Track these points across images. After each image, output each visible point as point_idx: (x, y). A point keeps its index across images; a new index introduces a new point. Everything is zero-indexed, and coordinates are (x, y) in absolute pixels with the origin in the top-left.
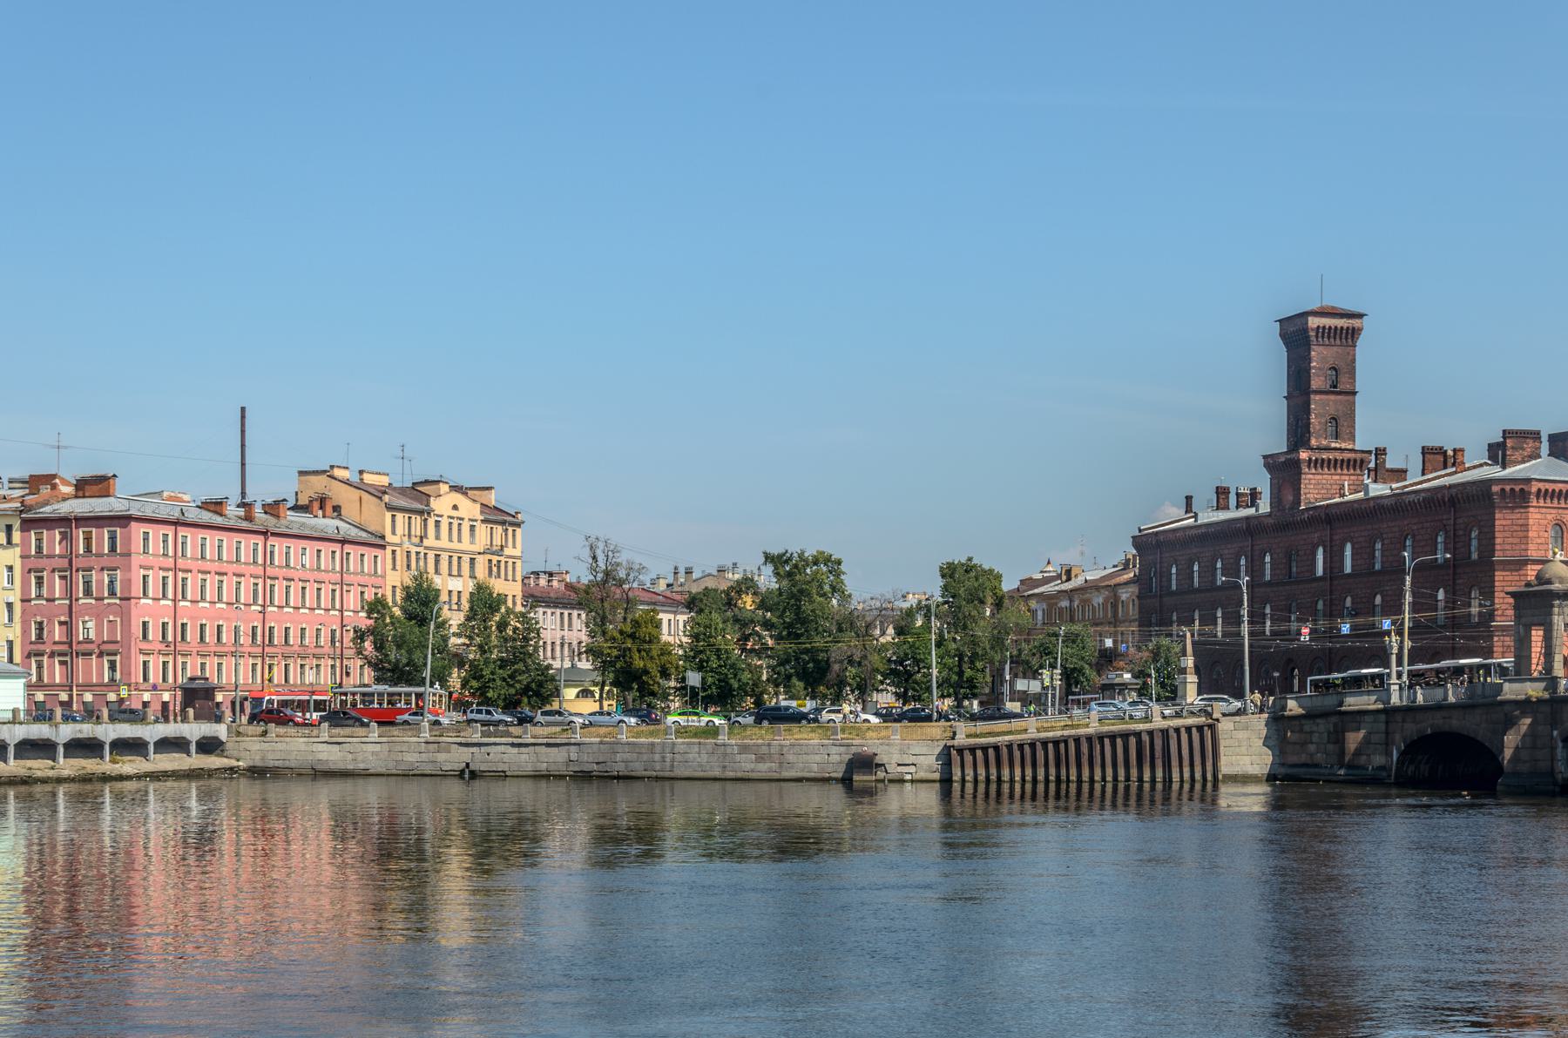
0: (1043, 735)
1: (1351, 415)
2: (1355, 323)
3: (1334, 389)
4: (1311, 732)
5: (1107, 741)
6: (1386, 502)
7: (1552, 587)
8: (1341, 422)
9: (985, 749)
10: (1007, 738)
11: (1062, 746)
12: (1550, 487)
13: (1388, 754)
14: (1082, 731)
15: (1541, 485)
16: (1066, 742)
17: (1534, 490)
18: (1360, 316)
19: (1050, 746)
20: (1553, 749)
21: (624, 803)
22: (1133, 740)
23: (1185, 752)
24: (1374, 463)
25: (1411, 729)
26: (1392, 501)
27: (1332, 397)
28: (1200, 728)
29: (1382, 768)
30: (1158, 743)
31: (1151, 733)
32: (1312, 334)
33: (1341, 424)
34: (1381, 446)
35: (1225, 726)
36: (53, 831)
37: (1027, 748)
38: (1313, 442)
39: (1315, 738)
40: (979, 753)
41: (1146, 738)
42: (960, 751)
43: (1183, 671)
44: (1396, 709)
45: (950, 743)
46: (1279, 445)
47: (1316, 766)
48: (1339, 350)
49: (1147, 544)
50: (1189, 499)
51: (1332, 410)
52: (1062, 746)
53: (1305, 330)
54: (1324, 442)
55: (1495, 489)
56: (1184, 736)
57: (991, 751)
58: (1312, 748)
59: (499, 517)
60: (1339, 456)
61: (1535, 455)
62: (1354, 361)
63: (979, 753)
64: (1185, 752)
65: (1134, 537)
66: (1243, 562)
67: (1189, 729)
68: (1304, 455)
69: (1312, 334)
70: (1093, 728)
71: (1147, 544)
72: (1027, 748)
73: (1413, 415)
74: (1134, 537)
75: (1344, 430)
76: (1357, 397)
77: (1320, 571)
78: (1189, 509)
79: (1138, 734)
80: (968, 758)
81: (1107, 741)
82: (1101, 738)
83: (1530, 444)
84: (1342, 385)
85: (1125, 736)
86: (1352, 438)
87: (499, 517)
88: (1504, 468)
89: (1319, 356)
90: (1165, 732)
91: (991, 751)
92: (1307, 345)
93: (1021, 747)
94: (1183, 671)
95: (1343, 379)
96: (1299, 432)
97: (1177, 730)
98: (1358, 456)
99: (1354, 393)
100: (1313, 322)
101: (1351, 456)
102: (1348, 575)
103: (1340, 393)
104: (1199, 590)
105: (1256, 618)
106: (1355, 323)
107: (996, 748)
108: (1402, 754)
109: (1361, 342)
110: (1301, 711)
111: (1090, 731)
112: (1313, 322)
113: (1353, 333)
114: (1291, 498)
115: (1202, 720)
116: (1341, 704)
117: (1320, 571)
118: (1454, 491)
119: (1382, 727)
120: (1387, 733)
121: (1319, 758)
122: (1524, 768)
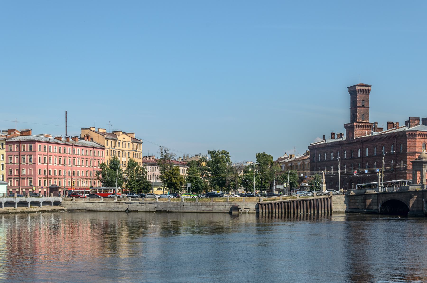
0: (284, 200)
1: (368, 113)
2: (369, 88)
3: (363, 106)
4: (357, 200)
5: (301, 202)
6: (377, 137)
7: (423, 160)
8: (365, 115)
9: (268, 204)
10: (274, 201)
11: (289, 203)
12: (422, 133)
13: (378, 206)
14: (295, 199)
15: (420, 132)
16: (290, 202)
17: (418, 133)
18: (370, 86)
19: (286, 203)
20: (423, 204)
22: (308, 202)
23: (323, 205)
24: (374, 126)
25: (384, 199)
26: (379, 137)
27: (363, 108)
28: (327, 199)
29: (376, 209)
30: (315, 202)
31: (313, 200)
32: (357, 91)
33: (365, 116)
34: (376, 122)
35: (334, 198)
37: (280, 204)
38: (358, 121)
39: (358, 201)
40: (267, 205)
41: (312, 201)
42: (262, 205)
43: (322, 183)
44: (380, 193)
45: (259, 203)
46: (348, 121)
47: (358, 209)
48: (365, 95)
49: (312, 148)
50: (324, 136)
51: (363, 112)
52: (289, 203)
53: (355, 90)
54: (361, 121)
55: (407, 133)
56: (322, 201)
57: (270, 205)
58: (357, 204)
59: (136, 141)
60: (365, 124)
61: (418, 124)
62: (369, 98)
63: (267, 205)
64: (323, 205)
65: (309, 147)
66: (338, 153)
67: (324, 199)
68: (355, 124)
69: (357, 91)
70: (298, 198)
71: (312, 148)
72: (280, 204)
73: (385, 113)
74: (309, 147)
75: (366, 117)
76: (370, 108)
77: (359, 156)
78: (324, 139)
79: (310, 200)
80: (264, 207)
81: (301, 202)
82: (300, 201)
83: (417, 121)
84: (365, 105)
85: (306, 201)
86: (368, 119)
87: (136, 141)
88: (410, 127)
89: (359, 97)
90: (317, 200)
91: (270, 205)
92: (356, 94)
93: (278, 204)
94: (322, 183)
95: (366, 103)
96: (354, 118)
97: (321, 199)
98: (370, 124)
99: (369, 107)
100: (358, 88)
101: (368, 124)
102: (367, 157)
103: (365, 107)
104: (327, 161)
105: (342, 168)
106: (369, 88)
107: (271, 204)
108: (382, 206)
109: (371, 93)
110: (354, 194)
111: (297, 199)
112: (358, 88)
113: (369, 91)
114: (352, 136)
115: (327, 196)
116: (365, 192)
117: (359, 156)
118: (396, 134)
119: (376, 198)
120: (378, 200)
121: (359, 207)
122: (415, 209)
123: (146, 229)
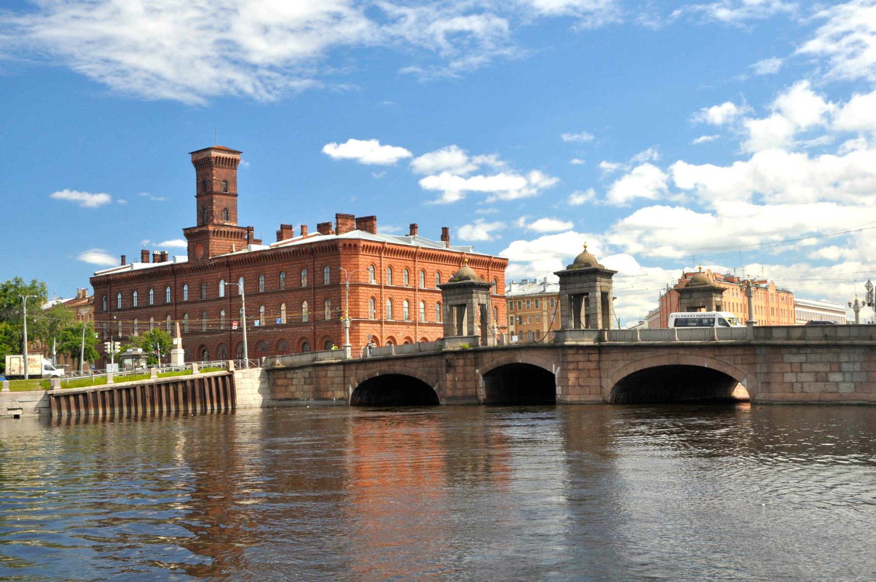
0: (119, 385)
1: (235, 208)
2: (237, 157)
3: (225, 192)
4: (292, 379)
5: (163, 388)
6: (268, 253)
8: (230, 211)
9: (76, 395)
10: (93, 387)
11: (132, 392)
12: (369, 244)
13: (346, 390)
14: (146, 381)
15: (366, 243)
17: (362, 245)
18: (239, 153)
19: (124, 392)
20: (477, 381)
21: (72, 476)
22: (180, 387)
24: (246, 235)
25: (364, 374)
26: (272, 252)
28: (223, 377)
29: (342, 399)
30: (197, 387)
31: (192, 381)
33: (229, 213)
34: (251, 225)
36: (586, 310)
37: (107, 394)
38: (215, 221)
39: (295, 382)
40: (72, 399)
41: (189, 384)
43: (176, 347)
44: (351, 363)
45: (50, 392)
46: (193, 222)
47: (296, 399)
48: (228, 171)
50: (123, 257)
52: (132, 392)
54: (221, 222)
55: (341, 244)
57: (81, 397)
58: (293, 388)
60: (230, 230)
62: (236, 177)
63: (72, 399)
65: (91, 278)
67: (216, 378)
68: (211, 228)
72: (107, 394)
74: (91, 278)
75: (231, 215)
76: (238, 198)
77: (222, 294)
78: (123, 263)
79: (184, 382)
80: (63, 402)
81: (163, 388)
82: (159, 385)
85: (175, 383)
86: (236, 221)
89: (218, 174)
90: (201, 380)
91: (81, 397)
93: (103, 393)
94: (176, 347)
95: (231, 187)
96: (204, 213)
97: (209, 379)
98: (240, 230)
99: (236, 195)
100: (214, 154)
101: (236, 230)
102: (222, 298)
103: (227, 195)
104: (137, 308)
106: (237, 157)
107: (85, 394)
108: (356, 390)
110: (281, 366)
113: (235, 162)
114: (202, 253)
117: (222, 294)
119: (342, 373)
120: (344, 377)
121: (298, 394)
122: (459, 393)
123: (339, 487)
